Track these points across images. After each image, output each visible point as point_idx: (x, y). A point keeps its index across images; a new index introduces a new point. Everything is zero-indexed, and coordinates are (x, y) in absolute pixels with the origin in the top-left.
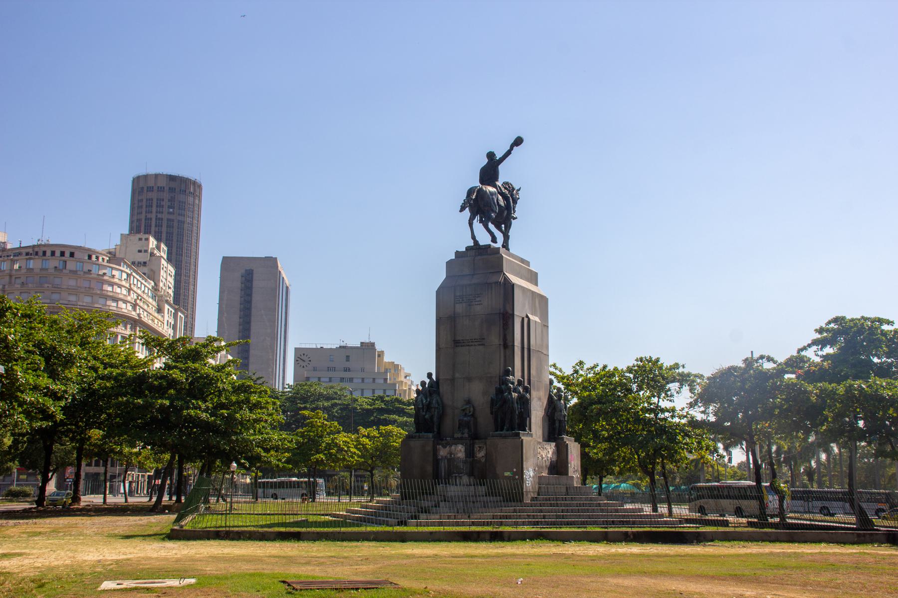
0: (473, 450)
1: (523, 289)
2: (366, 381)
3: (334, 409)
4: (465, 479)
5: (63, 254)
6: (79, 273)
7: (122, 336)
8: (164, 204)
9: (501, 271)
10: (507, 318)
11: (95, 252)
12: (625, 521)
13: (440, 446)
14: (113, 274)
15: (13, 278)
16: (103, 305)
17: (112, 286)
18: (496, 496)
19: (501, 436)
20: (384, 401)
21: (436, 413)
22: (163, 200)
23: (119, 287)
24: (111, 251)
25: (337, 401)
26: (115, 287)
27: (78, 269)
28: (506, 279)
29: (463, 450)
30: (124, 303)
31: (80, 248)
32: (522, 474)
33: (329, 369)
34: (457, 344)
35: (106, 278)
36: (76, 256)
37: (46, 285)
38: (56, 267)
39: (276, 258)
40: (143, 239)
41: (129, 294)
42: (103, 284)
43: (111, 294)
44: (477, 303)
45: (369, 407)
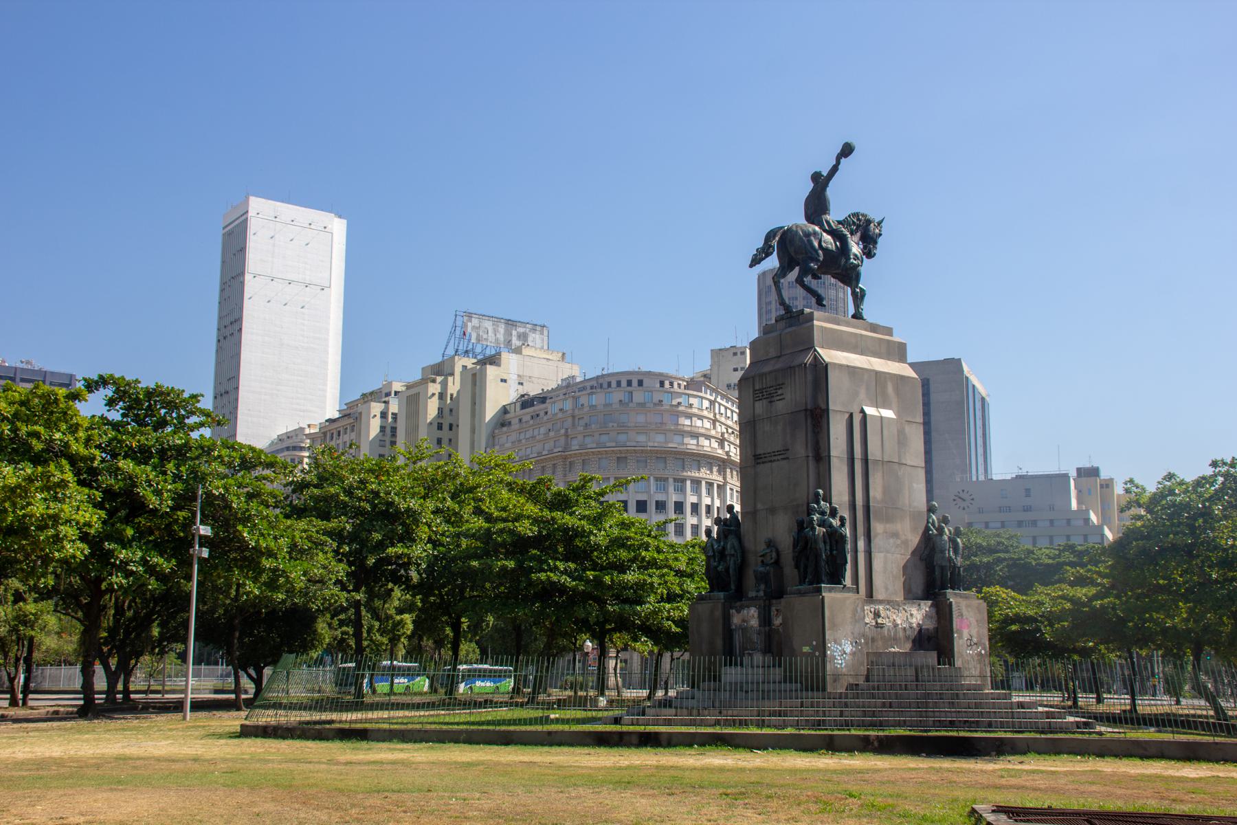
0: (770, 613)
1: (852, 371)
3: (998, 566)
4: (758, 658)
5: (629, 383)
6: (648, 405)
7: (706, 482)
9: (811, 347)
10: (817, 416)
11: (667, 377)
12: (973, 722)
13: (734, 611)
15: (577, 418)
16: (679, 444)
18: (791, 682)
19: (800, 593)
20: (1076, 551)
21: (732, 562)
22: (796, 299)
24: (705, 373)
25: (1002, 555)
26: (694, 419)
28: (817, 359)
29: (756, 615)
30: (706, 439)
31: (649, 373)
32: (823, 646)
33: (1000, 510)
34: (759, 461)
35: (681, 408)
36: (645, 384)
37: (611, 424)
38: (621, 401)
40: (739, 354)
41: (714, 428)
42: (678, 416)
44: (778, 398)
45: (1050, 561)
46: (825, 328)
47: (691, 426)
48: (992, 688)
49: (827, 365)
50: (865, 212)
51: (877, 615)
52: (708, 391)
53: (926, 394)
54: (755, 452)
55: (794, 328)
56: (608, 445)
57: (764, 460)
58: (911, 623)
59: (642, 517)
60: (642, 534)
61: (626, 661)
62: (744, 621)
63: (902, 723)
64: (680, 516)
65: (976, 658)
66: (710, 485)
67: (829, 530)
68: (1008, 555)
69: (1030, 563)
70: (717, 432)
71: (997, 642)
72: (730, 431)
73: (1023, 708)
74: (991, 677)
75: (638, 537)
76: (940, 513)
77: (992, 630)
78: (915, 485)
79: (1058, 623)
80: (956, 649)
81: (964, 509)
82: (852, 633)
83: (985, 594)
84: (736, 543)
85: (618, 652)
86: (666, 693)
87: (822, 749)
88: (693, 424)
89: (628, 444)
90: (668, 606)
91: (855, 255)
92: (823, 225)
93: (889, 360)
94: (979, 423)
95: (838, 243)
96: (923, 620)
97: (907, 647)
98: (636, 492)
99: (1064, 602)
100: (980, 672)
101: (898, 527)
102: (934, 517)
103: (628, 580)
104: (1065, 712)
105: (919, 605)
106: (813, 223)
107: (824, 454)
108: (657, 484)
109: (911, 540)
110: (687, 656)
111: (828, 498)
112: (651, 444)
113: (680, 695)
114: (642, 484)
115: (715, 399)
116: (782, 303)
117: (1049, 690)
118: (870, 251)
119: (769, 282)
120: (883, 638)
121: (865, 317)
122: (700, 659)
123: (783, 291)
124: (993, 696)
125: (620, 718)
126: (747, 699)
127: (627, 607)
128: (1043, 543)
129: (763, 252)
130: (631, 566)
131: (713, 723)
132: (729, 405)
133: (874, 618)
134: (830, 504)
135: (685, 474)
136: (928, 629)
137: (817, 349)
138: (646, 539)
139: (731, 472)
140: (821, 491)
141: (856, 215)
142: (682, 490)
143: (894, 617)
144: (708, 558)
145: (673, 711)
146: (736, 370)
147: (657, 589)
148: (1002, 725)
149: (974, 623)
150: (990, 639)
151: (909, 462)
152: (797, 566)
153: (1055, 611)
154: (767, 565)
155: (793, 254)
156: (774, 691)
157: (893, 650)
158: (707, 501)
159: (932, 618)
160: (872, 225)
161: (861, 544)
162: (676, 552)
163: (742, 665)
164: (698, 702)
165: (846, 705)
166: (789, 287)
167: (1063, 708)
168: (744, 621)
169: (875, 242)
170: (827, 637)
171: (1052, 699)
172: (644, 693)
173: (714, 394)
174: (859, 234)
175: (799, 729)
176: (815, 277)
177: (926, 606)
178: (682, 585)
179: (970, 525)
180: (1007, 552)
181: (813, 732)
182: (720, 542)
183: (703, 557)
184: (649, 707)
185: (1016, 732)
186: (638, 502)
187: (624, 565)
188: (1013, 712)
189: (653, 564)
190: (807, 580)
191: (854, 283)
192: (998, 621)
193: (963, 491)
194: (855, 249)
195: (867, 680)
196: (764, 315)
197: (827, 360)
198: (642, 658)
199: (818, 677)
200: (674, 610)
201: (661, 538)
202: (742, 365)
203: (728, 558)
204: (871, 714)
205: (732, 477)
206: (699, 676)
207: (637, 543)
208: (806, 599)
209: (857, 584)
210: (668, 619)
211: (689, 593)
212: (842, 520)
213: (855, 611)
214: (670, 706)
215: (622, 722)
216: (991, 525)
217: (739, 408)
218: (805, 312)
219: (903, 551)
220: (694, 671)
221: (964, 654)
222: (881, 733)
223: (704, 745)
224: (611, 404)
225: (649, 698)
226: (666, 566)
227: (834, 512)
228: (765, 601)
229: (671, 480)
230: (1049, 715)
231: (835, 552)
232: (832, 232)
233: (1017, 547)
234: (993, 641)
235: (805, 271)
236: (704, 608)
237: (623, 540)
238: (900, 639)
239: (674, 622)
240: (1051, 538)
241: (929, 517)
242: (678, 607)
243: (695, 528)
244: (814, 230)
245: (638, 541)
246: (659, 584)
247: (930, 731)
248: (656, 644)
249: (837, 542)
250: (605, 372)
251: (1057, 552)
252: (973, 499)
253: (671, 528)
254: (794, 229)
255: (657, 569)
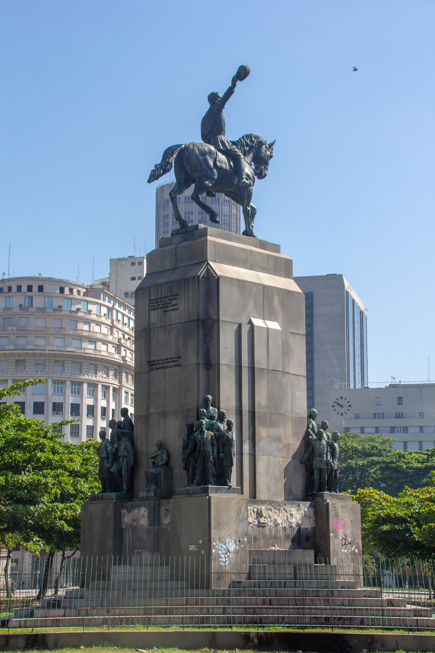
0: (159, 513)
2: (425, 430)
4: (147, 556)
5: (30, 288)
6: (47, 310)
7: (103, 386)
8: (194, 218)
11: (67, 283)
12: (347, 619)
13: (125, 510)
14: (89, 309)
17: (89, 324)
18: (177, 580)
19: (188, 494)
21: (124, 464)
22: (192, 213)
23: (97, 325)
24: (104, 281)
25: (376, 459)
26: (92, 325)
27: (46, 306)
28: (210, 272)
29: (146, 514)
30: (103, 344)
31: (49, 280)
33: (375, 416)
35: (80, 314)
37: (10, 328)
38: (21, 305)
39: (341, 275)
40: (137, 264)
41: (112, 334)
43: (87, 334)
44: (172, 308)
45: (420, 465)
46: (218, 243)
47: (89, 331)
48: (365, 585)
49: (218, 278)
50: (258, 135)
51: (259, 515)
52: (107, 298)
53: (310, 307)
54: (149, 358)
55: (188, 243)
56: (7, 347)
57: (158, 366)
58: (291, 523)
59: (39, 418)
60: (38, 435)
61: (16, 561)
62: (134, 520)
63: (281, 620)
64: (76, 418)
65: (350, 557)
66: (106, 388)
67: (217, 433)
68: (381, 458)
69: (401, 466)
70: (114, 338)
71: (369, 541)
72: (127, 337)
73: (393, 606)
74: (364, 575)
75: (34, 438)
76: (320, 419)
77: (366, 529)
78: (297, 393)
79: (426, 524)
80: (331, 548)
81: (342, 414)
82: (236, 532)
83: (360, 495)
84: (129, 446)
85: (9, 552)
86: (56, 592)
87: (205, 647)
88: (92, 330)
89: (27, 347)
90: (61, 506)
91: (248, 175)
92: (219, 145)
93: (276, 275)
94: (358, 335)
95: (232, 163)
96: (302, 520)
97: (287, 546)
98: (34, 394)
99: (431, 504)
100: (354, 571)
101: (280, 431)
102: (314, 423)
103: (22, 481)
104: (431, 611)
105: (299, 506)
106: (209, 143)
107: (214, 362)
108: (55, 387)
109: (293, 444)
110: (78, 554)
111: (216, 404)
112: (50, 348)
113: (69, 596)
114: (40, 386)
115: (113, 306)
116: (178, 218)
117: (416, 588)
118: (261, 172)
119: (167, 196)
120: (265, 537)
121: (255, 234)
122: (187, 559)
123: (179, 205)
124: (365, 594)
125: (8, 621)
126: (134, 597)
127: (20, 507)
128: (413, 447)
129: (161, 168)
130: (26, 467)
131: (101, 622)
132: (126, 312)
133: (257, 518)
134: (219, 409)
135: (82, 377)
136: (306, 529)
137: (210, 263)
138: (42, 440)
139: (127, 376)
140: (210, 397)
141: (249, 136)
142: (79, 393)
143: (276, 517)
144: (102, 460)
145: (62, 611)
146: (133, 279)
147: (51, 489)
148: (373, 623)
149: (349, 523)
150: (363, 538)
151: (292, 372)
152: (186, 468)
153: (423, 512)
154: (158, 466)
155: (189, 172)
156: (161, 589)
157: (273, 548)
158: (102, 403)
159: (310, 518)
160: (264, 147)
161: (246, 447)
162: (71, 453)
163: (130, 563)
164: (87, 601)
165: (229, 602)
166: (185, 202)
167: (429, 605)
168: (134, 520)
169: (267, 164)
170: (212, 536)
171: (419, 596)
172: (34, 593)
173: (112, 302)
174: (251, 155)
175: (184, 627)
176: (210, 194)
177: (305, 506)
178: (76, 485)
179: (347, 429)
180: (380, 455)
181: (197, 630)
182: (114, 444)
183: (97, 458)
184: (38, 608)
185: (386, 629)
186: (36, 404)
187: (18, 466)
188: (383, 610)
189: (48, 464)
190: (195, 481)
191: (246, 201)
192: (370, 521)
193: (341, 398)
194: (248, 169)
195: (249, 578)
196: (162, 228)
197: (219, 273)
198: (33, 557)
199: (203, 575)
200: (67, 509)
201: (57, 439)
202: (139, 275)
203: (121, 460)
204: (252, 611)
205: (127, 381)
206: (88, 575)
207: (32, 444)
208: (194, 499)
209: (242, 486)
210: (61, 519)
211: (82, 492)
212: (229, 424)
213: (239, 511)
214: (59, 607)
215: (9, 625)
216: (366, 430)
217: (136, 316)
218: (199, 227)
219: (284, 455)
220: (84, 571)
221: (339, 553)
222: (261, 630)
223: (91, 646)
224: (11, 309)
225: (38, 598)
226: (61, 467)
227: (221, 417)
228: (154, 501)
229: (68, 383)
230: (416, 613)
231: (221, 455)
232: (227, 153)
233: (389, 451)
234: (367, 540)
235: (200, 189)
236: (96, 508)
237: (19, 441)
238: (280, 538)
239: (66, 521)
240: (421, 443)
241: (309, 423)
242: (71, 507)
243: (91, 430)
244: (210, 150)
245: (34, 442)
246: (54, 484)
247: (306, 628)
248: (48, 543)
249: (224, 445)
250: (6, 277)
251: (425, 457)
252: (350, 406)
253: (67, 429)
254: (191, 147)
255: (52, 470)
